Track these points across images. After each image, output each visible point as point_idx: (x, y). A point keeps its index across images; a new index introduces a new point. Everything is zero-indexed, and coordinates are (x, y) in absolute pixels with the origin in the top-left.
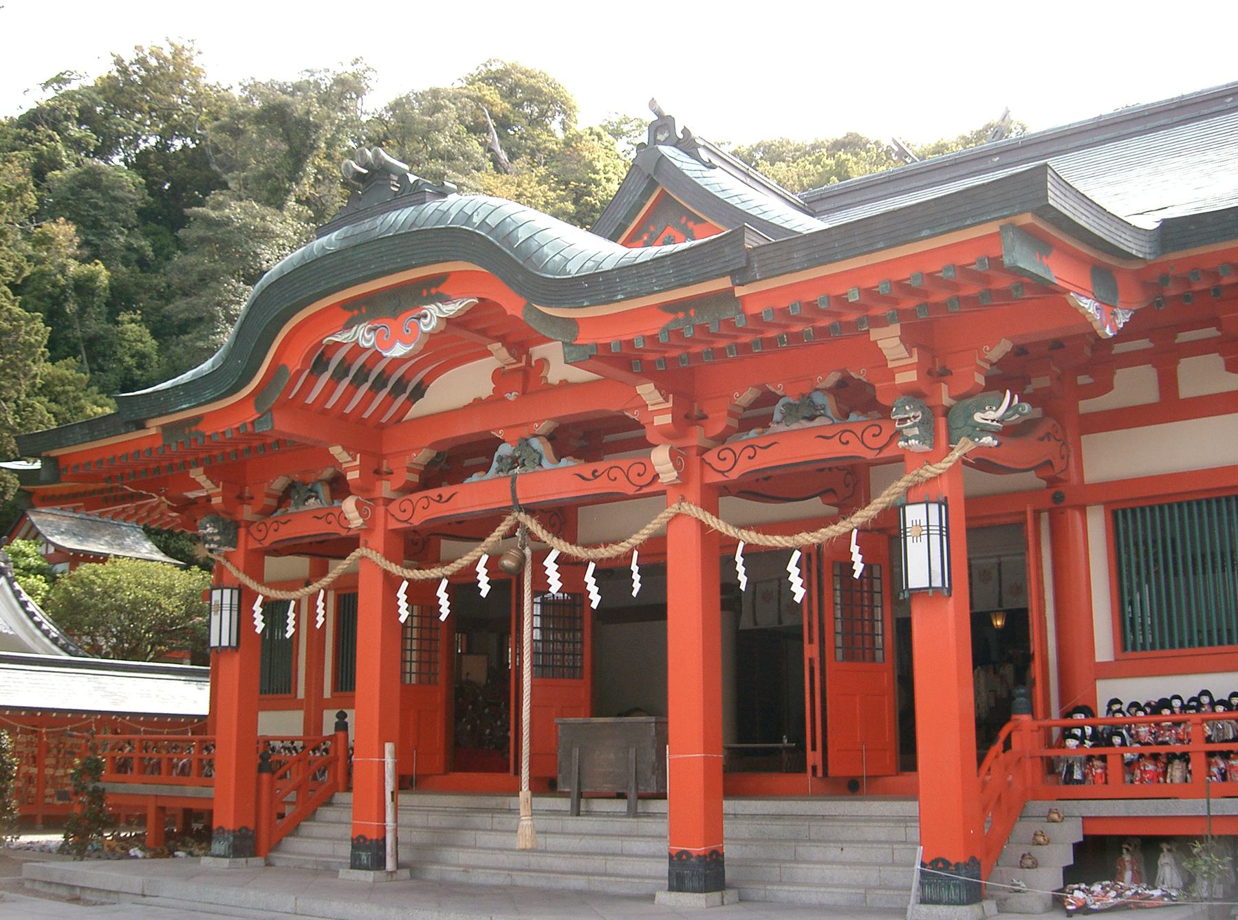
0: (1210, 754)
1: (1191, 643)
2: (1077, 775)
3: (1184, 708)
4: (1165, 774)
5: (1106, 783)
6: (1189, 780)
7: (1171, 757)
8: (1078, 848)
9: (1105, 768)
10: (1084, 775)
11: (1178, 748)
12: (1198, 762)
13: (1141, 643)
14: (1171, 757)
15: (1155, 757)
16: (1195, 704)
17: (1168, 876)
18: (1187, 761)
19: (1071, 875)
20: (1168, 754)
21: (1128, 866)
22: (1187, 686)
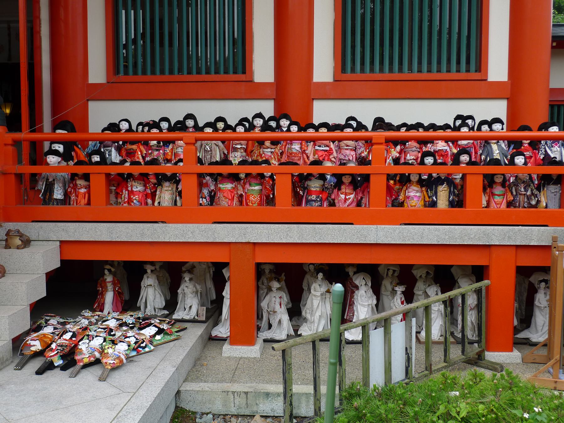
0: (201, 176)
1: (180, 70)
2: (58, 194)
3: (171, 129)
4: (153, 196)
5: (89, 203)
6: (179, 204)
7: (162, 178)
8: (52, 278)
9: (88, 187)
10: (67, 195)
11: (168, 168)
12: (189, 185)
13: (132, 73)
14: (162, 178)
15: (144, 177)
16: (180, 126)
17: (151, 298)
18: (177, 182)
19: (39, 310)
20: (157, 175)
21: (110, 287)
22: (175, 110)
